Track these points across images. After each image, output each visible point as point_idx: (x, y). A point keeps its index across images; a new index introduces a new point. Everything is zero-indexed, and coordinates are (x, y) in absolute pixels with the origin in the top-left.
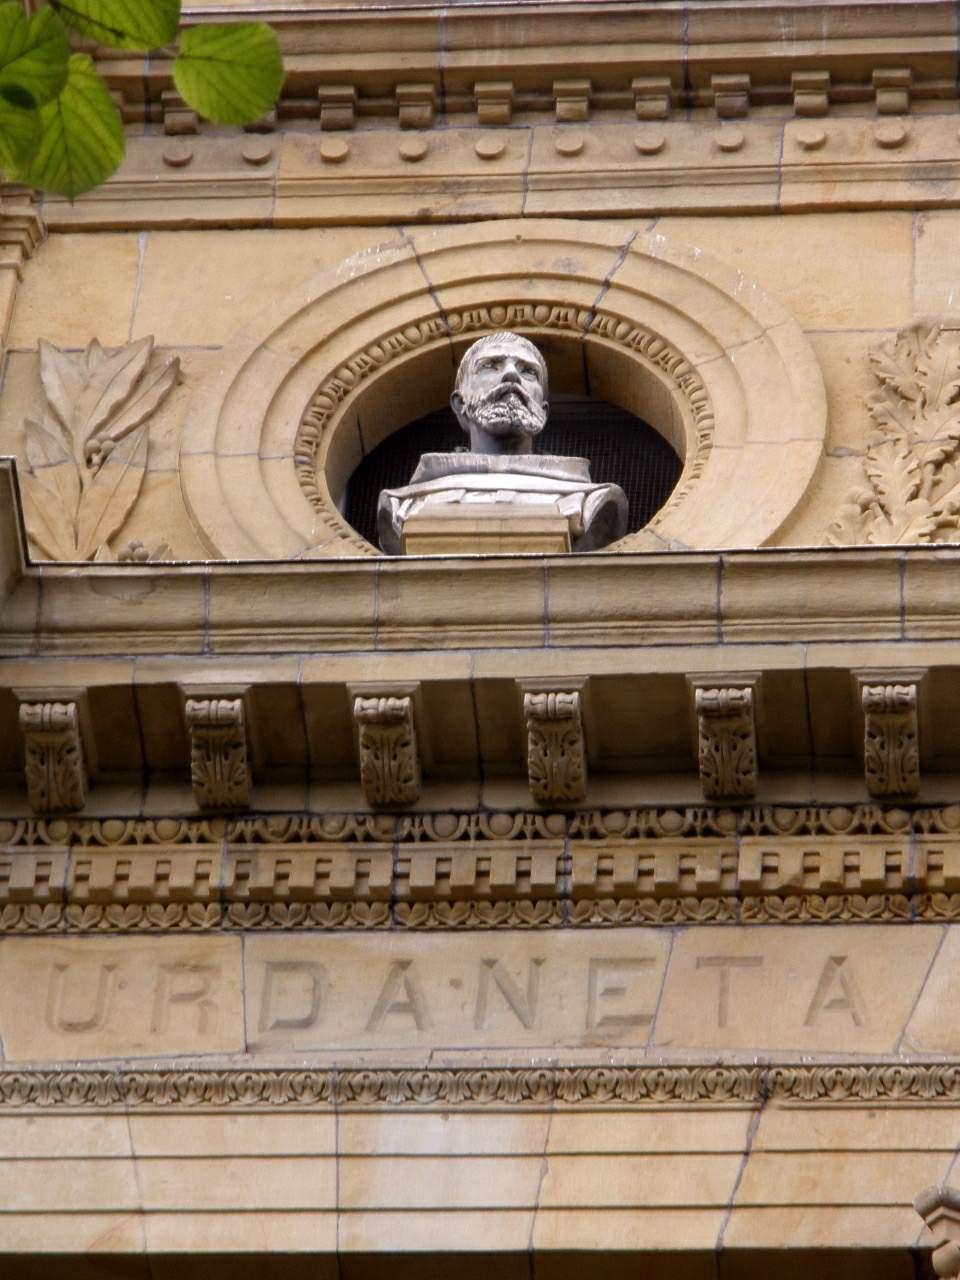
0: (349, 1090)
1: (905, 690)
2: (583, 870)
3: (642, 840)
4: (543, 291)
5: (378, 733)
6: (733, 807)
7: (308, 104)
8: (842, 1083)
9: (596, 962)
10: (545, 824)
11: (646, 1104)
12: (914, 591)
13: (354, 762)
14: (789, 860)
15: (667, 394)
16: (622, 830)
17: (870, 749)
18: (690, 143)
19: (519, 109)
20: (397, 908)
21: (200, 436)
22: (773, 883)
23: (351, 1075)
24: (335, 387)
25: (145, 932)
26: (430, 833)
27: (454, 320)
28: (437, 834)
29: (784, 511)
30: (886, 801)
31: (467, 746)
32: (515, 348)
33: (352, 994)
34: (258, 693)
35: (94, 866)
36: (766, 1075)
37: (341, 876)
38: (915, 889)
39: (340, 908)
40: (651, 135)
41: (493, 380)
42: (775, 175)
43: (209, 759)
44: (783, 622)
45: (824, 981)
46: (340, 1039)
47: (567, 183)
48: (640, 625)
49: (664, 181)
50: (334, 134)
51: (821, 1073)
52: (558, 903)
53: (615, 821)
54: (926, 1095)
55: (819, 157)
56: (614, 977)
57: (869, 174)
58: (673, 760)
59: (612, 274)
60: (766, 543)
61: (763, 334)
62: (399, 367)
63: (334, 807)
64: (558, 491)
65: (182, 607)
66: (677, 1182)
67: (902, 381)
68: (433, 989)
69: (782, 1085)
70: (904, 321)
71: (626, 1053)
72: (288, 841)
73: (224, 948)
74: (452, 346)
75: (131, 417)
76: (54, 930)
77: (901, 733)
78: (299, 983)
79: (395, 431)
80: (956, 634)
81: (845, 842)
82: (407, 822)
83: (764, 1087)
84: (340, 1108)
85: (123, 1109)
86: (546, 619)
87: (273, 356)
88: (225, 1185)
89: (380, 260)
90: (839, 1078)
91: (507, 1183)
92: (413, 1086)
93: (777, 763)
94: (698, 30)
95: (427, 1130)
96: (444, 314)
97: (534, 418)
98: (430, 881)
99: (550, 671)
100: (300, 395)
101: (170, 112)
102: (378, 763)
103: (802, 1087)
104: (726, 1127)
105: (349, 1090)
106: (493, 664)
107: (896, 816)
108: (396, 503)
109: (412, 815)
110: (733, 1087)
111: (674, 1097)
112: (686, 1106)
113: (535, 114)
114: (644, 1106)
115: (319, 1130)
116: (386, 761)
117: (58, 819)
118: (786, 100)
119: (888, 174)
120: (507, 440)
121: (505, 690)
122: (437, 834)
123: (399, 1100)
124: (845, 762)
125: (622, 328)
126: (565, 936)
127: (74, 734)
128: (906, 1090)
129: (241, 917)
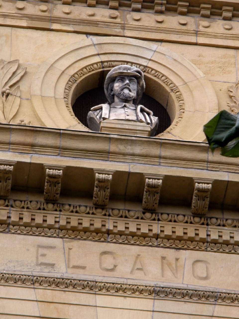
1: (159, 181)
3: (90, 215)
5: (199, 194)
7: (197, 9)
8: (72, 285)
9: (39, 246)
10: (15, 204)
11: (133, 295)
16: (183, 221)
19: (212, 14)
23: (50, 279)
25: (162, 247)
26: (193, 222)
27: (105, 64)
28: (195, 222)
30: (97, 206)
35: (235, 234)
36: (201, 293)
43: (199, 200)
47: (158, 30)
51: (116, 286)
52: (211, 244)
54: (162, 296)
55: (69, 16)
56: (45, 251)
59: (152, 57)
60: (203, 141)
62: (89, 76)
69: (221, 298)
72: (119, 217)
74: (103, 71)
76: (147, 245)
77: (105, 188)
80: (238, 172)
82: (154, 215)
84: (97, 293)
85: (33, 287)
90: (171, 291)
92: (50, 282)
96: (102, 62)
98: (53, 223)
101: (202, 10)
102: (149, 197)
103: (177, 294)
109: (156, 213)
110: (108, 288)
111: (108, 291)
112: (227, 304)
113: (100, 5)
114: (182, 300)
116: (201, 201)
117: (148, 212)
122: (195, 222)
123: (63, 287)
125: (153, 72)
127: (11, 176)
128: (90, 288)
129: (12, 229)
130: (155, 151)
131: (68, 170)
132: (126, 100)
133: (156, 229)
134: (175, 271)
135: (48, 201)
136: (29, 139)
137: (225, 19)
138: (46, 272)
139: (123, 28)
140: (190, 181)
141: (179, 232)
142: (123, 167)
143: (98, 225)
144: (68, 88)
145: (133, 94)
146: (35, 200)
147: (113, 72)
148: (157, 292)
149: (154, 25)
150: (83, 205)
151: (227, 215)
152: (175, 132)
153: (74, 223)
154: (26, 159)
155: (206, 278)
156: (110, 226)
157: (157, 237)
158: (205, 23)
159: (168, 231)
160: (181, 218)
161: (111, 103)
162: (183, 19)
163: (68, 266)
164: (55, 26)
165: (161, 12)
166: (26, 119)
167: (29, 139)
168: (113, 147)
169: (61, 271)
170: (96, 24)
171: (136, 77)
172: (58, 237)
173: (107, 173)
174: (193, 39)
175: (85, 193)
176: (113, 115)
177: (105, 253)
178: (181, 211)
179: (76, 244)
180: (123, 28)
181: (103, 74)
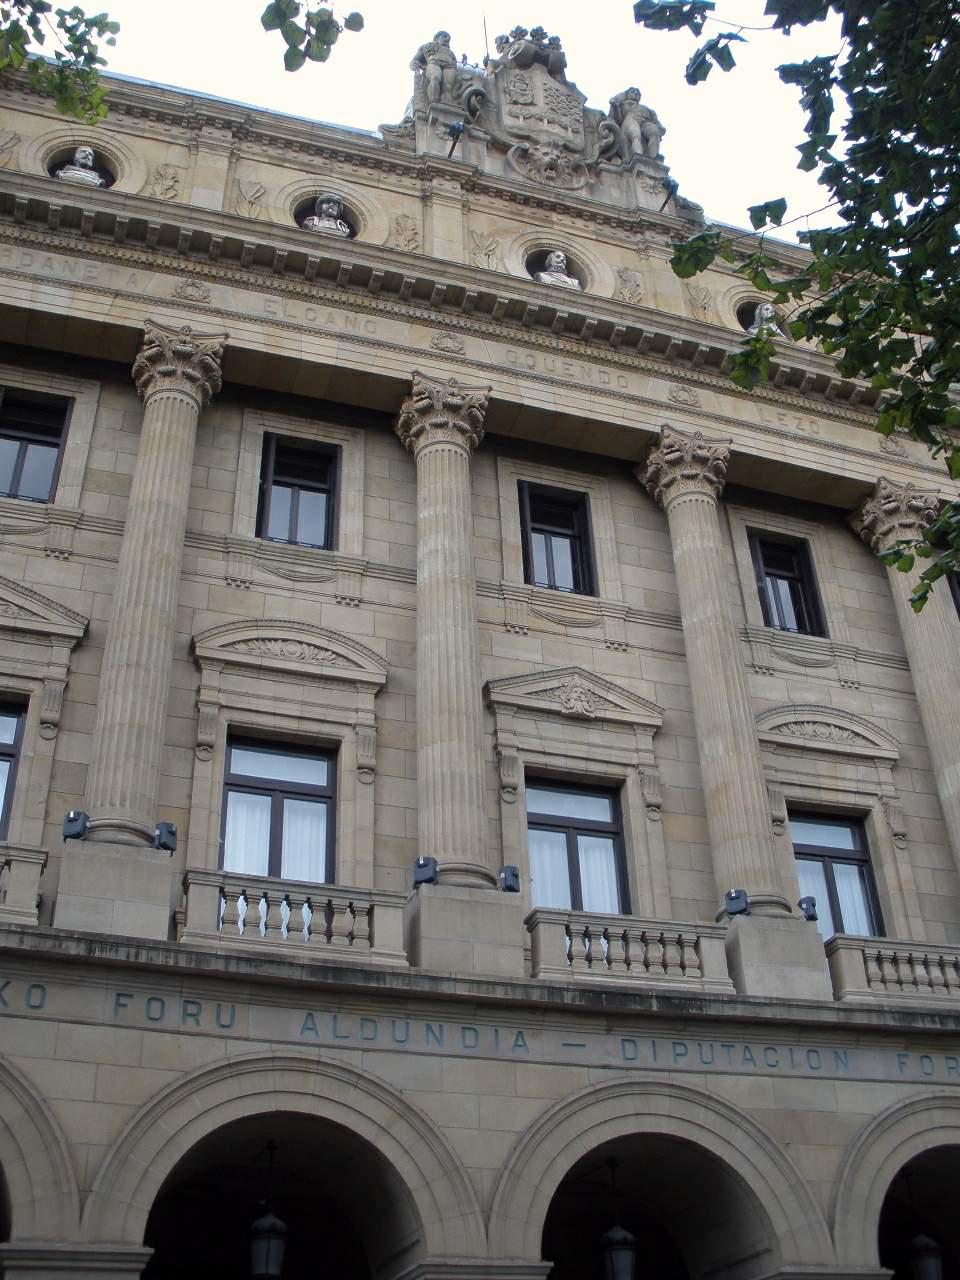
0: (36, 279)
2: (88, 248)
4: (95, 141)
6: (119, 242)
12: (163, 209)
13: (47, 216)
14: (128, 255)
15: (115, 167)
17: (148, 236)
18: (128, 120)
20: (50, 248)
21: (22, 153)
22: (124, 258)
24: (51, 149)
29: (139, 188)
30: (149, 247)
31: (70, 220)
32: (89, 150)
33: (39, 262)
34: (31, 200)
37: (41, 239)
38: (151, 264)
39: (39, 246)
40: (121, 117)
41: (83, 155)
42: (143, 130)
44: (137, 209)
45: (130, 278)
46: (36, 269)
48: (109, 204)
49: (122, 126)
50: (903, 627)
53: (96, 240)
56: (271, 304)
57: (161, 134)
58: (110, 231)
61: (137, 158)
63: (41, 226)
64: (92, 178)
65: (18, 180)
66: (97, 308)
67: (162, 173)
68: (56, 265)
70: (164, 162)
71: (91, 283)
73: (15, 249)
75: (9, 145)
78: (28, 258)
79: (62, 160)
81: (139, 253)
83: (117, 294)
86: (90, 198)
87: (406, 333)
88: (392, 364)
89: (63, 128)
91: (65, 302)
93: (128, 235)
94: (133, 99)
95: (50, 289)
97: (90, 163)
99: (90, 209)
100: (43, 150)
104: (109, 300)
105: (36, 279)
106: (581, 312)
107: (150, 250)
108: (61, 174)
113: (907, 646)
115: (30, 285)
118: (147, 117)
119: (166, 135)
120: (84, 166)
121: (80, 210)
124: (142, 238)
126: (82, 260)
130: (350, 247)
131: (291, 253)
132: (330, 216)
133: (344, 298)
134: (354, 326)
135: (275, 272)
136: (267, 230)
137: (398, 175)
138: (271, 317)
139: (331, 171)
140: (370, 270)
141: (359, 302)
142: (327, 255)
143: (306, 291)
144: (292, 204)
145: (335, 213)
146: (267, 271)
147: (322, 197)
148: (342, 337)
149: (351, 171)
150: (298, 277)
151: (391, 295)
152: (119, 186)
153: (291, 288)
154: (264, 242)
155: (374, 332)
156: (314, 293)
157: (344, 303)
158: (384, 175)
159: (352, 300)
160: (234, 267)
161: (320, 216)
162: (370, 171)
163: (285, 314)
164: (287, 165)
165: (357, 165)
166: (263, 218)
167: (267, 230)
168: (322, 242)
169: (280, 317)
170: (313, 166)
171: (337, 202)
172: (279, 296)
173: (156, 224)
174: (376, 184)
175: (300, 270)
176: (319, 224)
177: (310, 309)
178: (266, 269)
179: (291, 301)
180: (331, 171)
181: (314, 199)
